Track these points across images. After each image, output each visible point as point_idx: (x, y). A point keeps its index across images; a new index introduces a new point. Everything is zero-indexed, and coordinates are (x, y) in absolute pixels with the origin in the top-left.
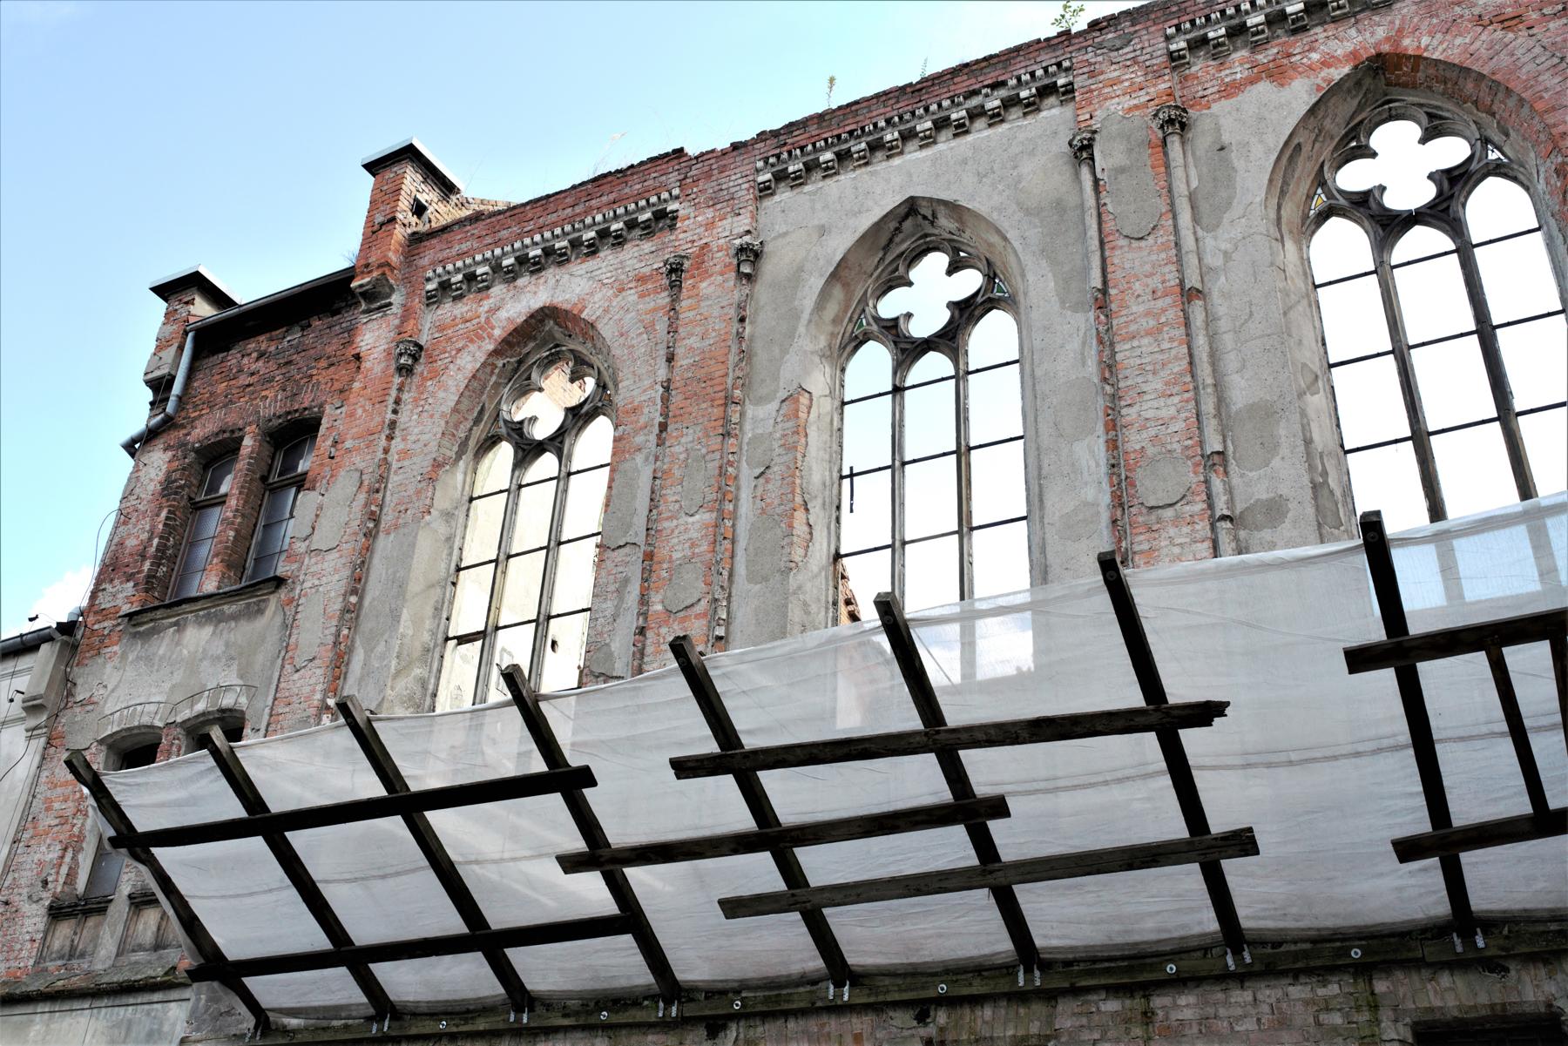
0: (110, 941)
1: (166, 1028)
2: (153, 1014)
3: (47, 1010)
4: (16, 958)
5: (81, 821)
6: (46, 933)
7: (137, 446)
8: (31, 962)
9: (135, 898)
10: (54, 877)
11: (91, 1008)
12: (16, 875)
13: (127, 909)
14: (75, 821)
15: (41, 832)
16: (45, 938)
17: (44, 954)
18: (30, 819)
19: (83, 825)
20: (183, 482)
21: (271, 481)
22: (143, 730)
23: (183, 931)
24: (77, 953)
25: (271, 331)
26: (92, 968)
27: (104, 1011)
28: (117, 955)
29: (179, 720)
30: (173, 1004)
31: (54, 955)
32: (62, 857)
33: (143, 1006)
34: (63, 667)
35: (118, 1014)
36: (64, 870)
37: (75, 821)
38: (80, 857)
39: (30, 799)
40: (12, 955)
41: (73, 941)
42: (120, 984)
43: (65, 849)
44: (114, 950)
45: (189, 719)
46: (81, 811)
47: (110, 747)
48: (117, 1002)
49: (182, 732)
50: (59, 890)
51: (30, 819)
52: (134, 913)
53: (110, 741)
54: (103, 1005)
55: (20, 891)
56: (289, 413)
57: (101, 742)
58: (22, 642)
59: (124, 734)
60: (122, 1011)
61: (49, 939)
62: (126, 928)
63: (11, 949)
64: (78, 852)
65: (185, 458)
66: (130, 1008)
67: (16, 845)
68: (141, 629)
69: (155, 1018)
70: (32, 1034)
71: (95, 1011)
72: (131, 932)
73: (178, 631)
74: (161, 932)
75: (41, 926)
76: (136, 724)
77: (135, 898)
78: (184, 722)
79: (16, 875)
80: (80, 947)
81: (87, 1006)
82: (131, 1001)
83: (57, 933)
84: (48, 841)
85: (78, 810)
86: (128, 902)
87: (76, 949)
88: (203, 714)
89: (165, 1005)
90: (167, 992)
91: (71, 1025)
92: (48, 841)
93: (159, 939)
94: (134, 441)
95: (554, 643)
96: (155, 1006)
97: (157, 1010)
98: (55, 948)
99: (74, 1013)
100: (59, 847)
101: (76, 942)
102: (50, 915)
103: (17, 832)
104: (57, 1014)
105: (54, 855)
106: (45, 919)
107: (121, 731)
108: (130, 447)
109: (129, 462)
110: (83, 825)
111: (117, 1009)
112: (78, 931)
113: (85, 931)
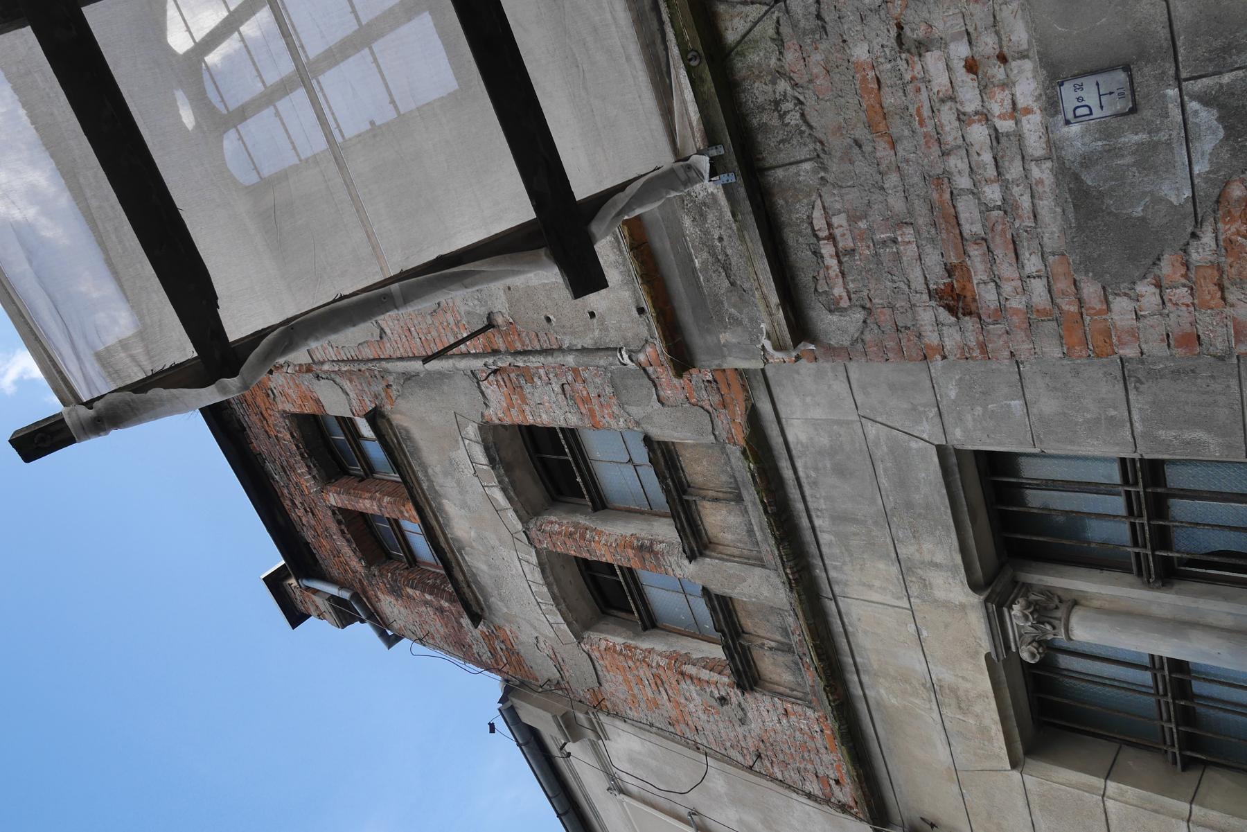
0: (749, 581)
1: (824, 441)
2: (813, 474)
3: (855, 678)
4: (813, 738)
5: (655, 657)
6: (774, 694)
7: (390, 633)
8: (809, 712)
9: (692, 550)
10: (713, 688)
11: (835, 598)
12: (728, 744)
13: (708, 560)
14: (654, 664)
15: (678, 712)
16: (781, 695)
17: (800, 695)
18: (671, 729)
19: (660, 654)
20: (389, 574)
21: (362, 473)
22: (551, 578)
23: (1095, 778)
24: (786, 641)
25: (279, 497)
26: (787, 607)
27: (833, 574)
28: (763, 566)
29: (520, 527)
30: (790, 438)
31: (800, 680)
32: (691, 677)
33: (809, 498)
34: (535, 695)
35: (830, 544)
36: (705, 674)
37: (654, 664)
38: (695, 656)
39: (654, 730)
40: (811, 745)
41: (771, 649)
42: (779, 542)
43: (682, 674)
44: (758, 571)
45: (516, 511)
46: (645, 657)
47: (588, 626)
48: (813, 549)
49: (533, 521)
50: (726, 680)
51: (671, 729)
52: (714, 550)
53: (576, 625)
54: (824, 575)
55: (741, 737)
56: (302, 455)
57: (579, 638)
58: (526, 744)
59: (563, 606)
60: (824, 538)
61: (782, 689)
62: (731, 558)
63: (804, 746)
64: (689, 659)
65: (374, 575)
66: (817, 522)
67: (701, 747)
68: (481, 599)
69: (816, 469)
70: (894, 701)
71: (837, 589)
72: (736, 552)
73: (464, 549)
74: (721, 495)
75: (767, 699)
76: (545, 589)
77: (692, 550)
78: (520, 518)
79: (728, 744)
80: (779, 638)
81: (831, 606)
82: (805, 522)
83: (775, 677)
84: (683, 701)
85: (644, 661)
86: (700, 559)
87: (782, 643)
88: (504, 490)
89: (794, 452)
90: (776, 453)
91: (865, 632)
92: (683, 701)
93: (728, 496)
94: (383, 634)
95: (641, 311)
96: (801, 474)
97: (806, 467)
98: (791, 678)
99: (850, 629)
100: (683, 684)
101: (773, 644)
102: (752, 689)
103: (687, 746)
104: (858, 660)
105: (690, 688)
106: (757, 695)
107: (560, 610)
108: (390, 641)
109: (312, 621)
110: (660, 654)
111: (825, 550)
112: (759, 642)
113: (761, 632)
